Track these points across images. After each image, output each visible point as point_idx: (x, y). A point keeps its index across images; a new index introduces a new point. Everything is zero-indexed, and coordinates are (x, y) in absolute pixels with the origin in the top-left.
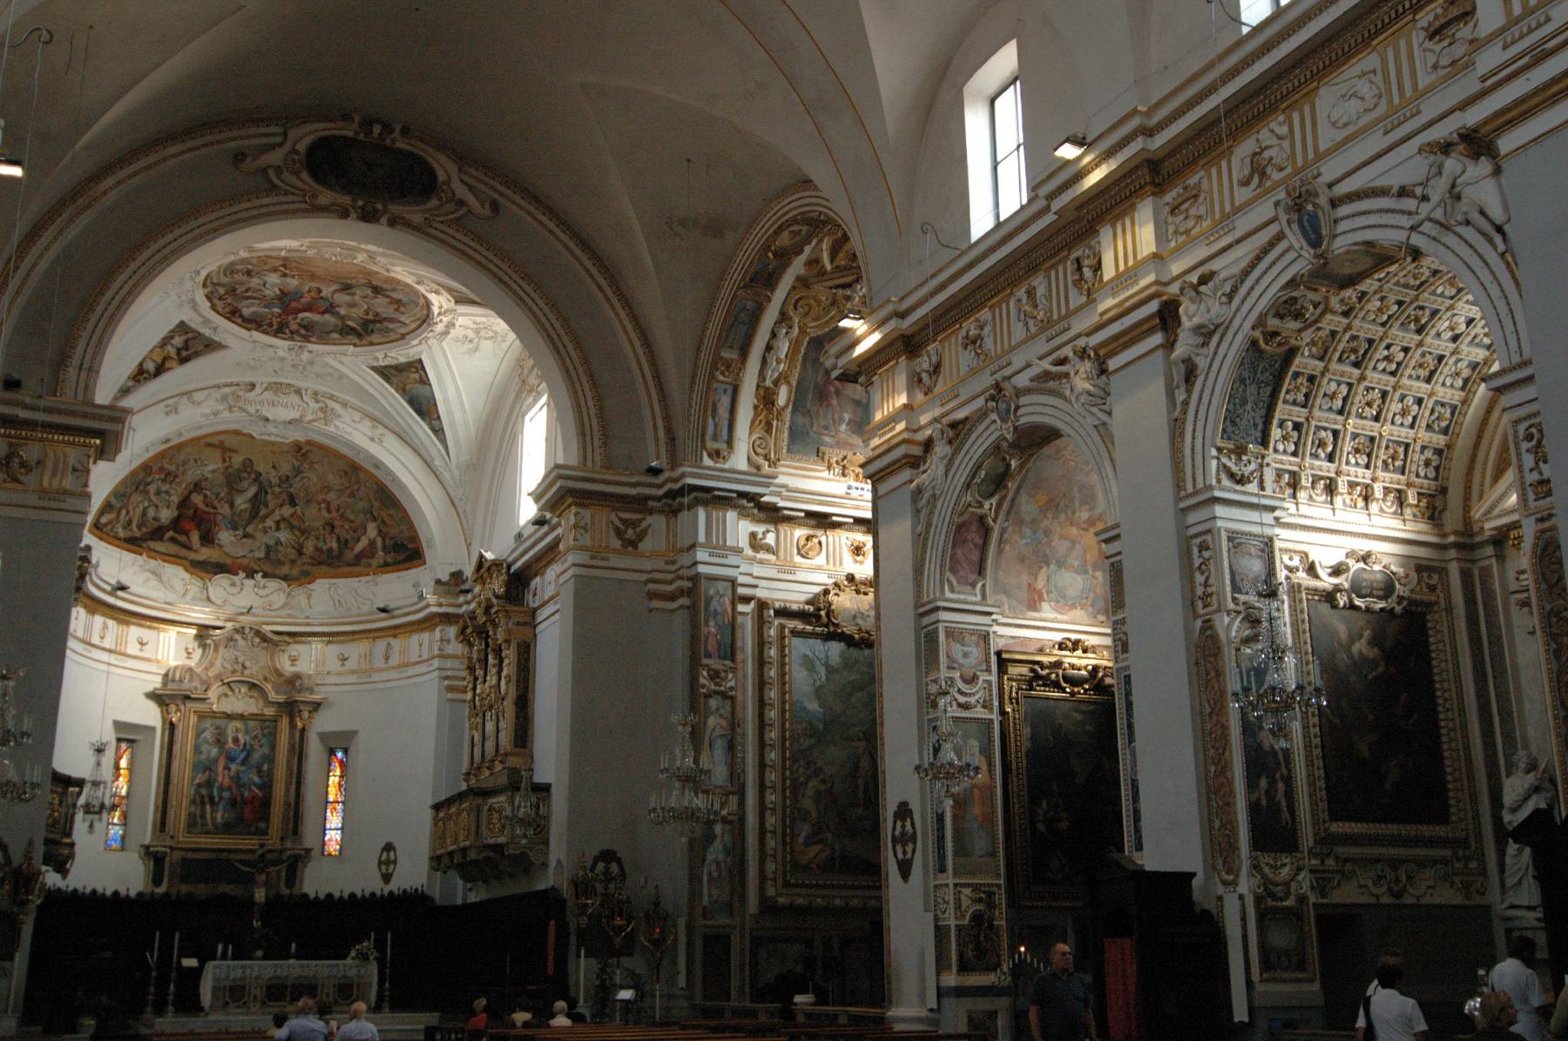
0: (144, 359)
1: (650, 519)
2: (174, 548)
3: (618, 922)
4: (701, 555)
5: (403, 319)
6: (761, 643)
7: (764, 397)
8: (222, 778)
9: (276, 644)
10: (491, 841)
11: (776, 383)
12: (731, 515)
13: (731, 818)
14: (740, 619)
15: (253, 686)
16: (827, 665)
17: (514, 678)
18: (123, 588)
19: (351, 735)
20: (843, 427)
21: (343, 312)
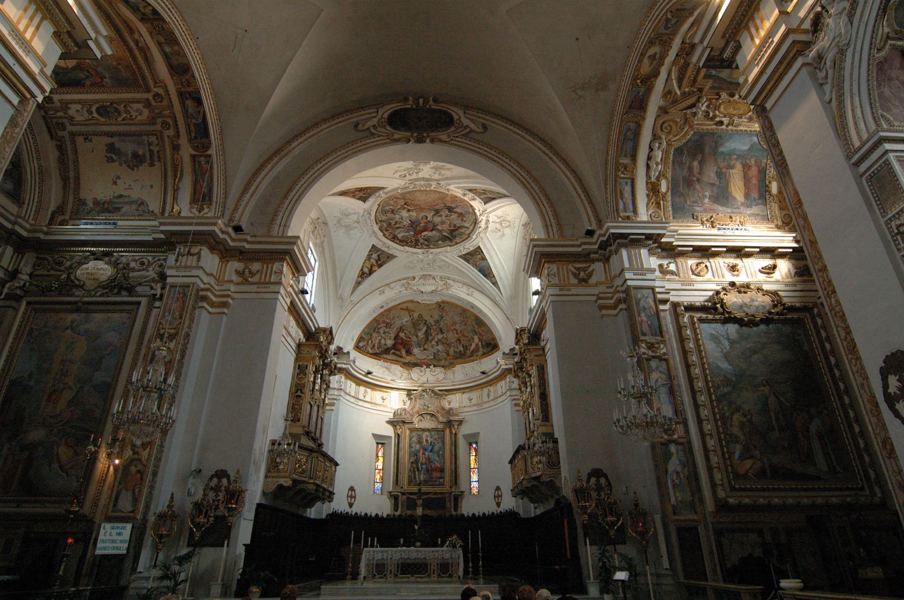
0: (363, 267)
1: (593, 266)
2: (395, 357)
3: (610, 519)
4: (628, 275)
5: (466, 225)
6: (679, 328)
7: (652, 190)
8: (422, 459)
9: (441, 396)
10: (534, 475)
11: (658, 179)
12: (644, 252)
13: (681, 440)
14: (662, 314)
15: (432, 415)
16: (728, 339)
17: (537, 384)
18: (370, 373)
19: (476, 435)
20: (706, 200)
21: (440, 228)
